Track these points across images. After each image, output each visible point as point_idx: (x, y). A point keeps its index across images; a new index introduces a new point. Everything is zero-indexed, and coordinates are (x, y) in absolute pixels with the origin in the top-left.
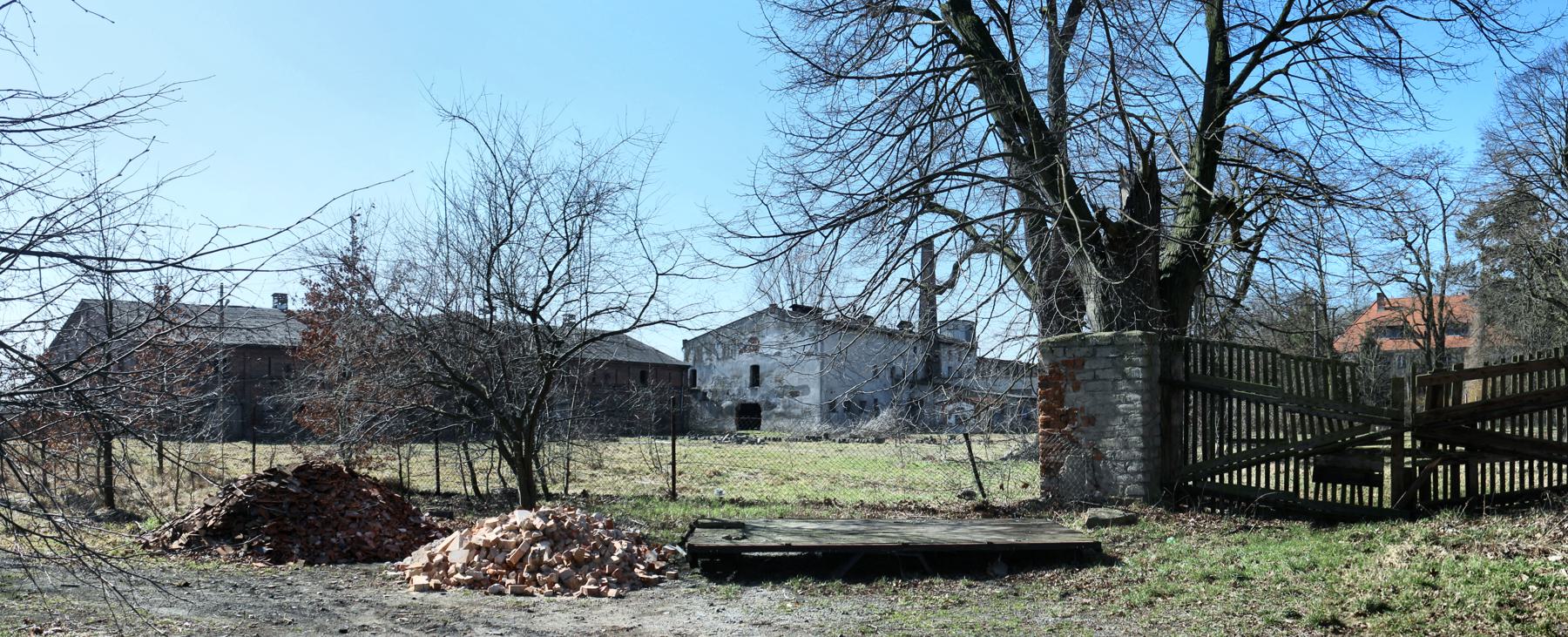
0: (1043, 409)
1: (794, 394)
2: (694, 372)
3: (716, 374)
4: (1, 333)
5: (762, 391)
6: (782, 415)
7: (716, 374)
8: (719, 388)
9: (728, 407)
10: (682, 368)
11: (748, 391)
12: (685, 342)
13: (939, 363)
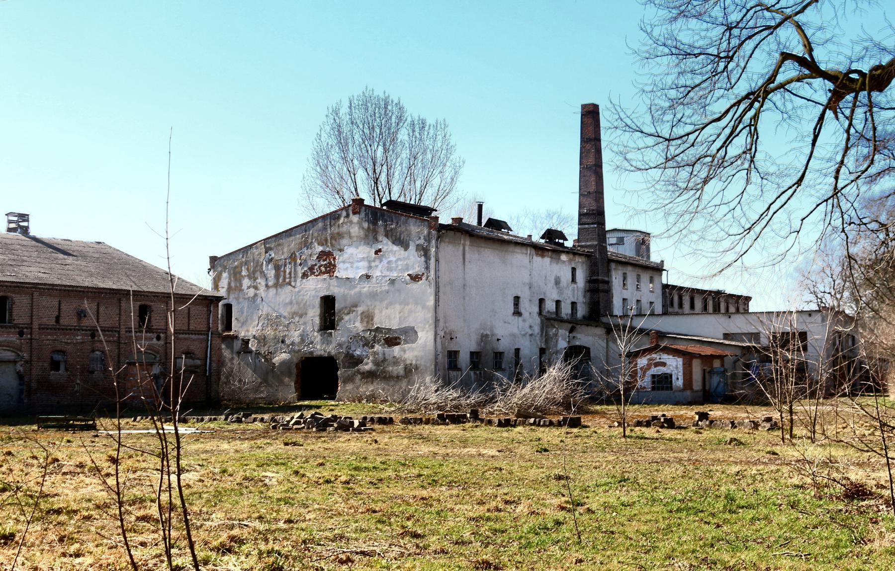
0: (149, 348)
1: (392, 342)
2: (228, 308)
3: (265, 309)
4: (890, 169)
5: (339, 336)
6: (370, 376)
7: (265, 309)
8: (269, 332)
9: (284, 363)
10: (210, 301)
11: (317, 337)
12: (213, 259)
13: (608, 292)
